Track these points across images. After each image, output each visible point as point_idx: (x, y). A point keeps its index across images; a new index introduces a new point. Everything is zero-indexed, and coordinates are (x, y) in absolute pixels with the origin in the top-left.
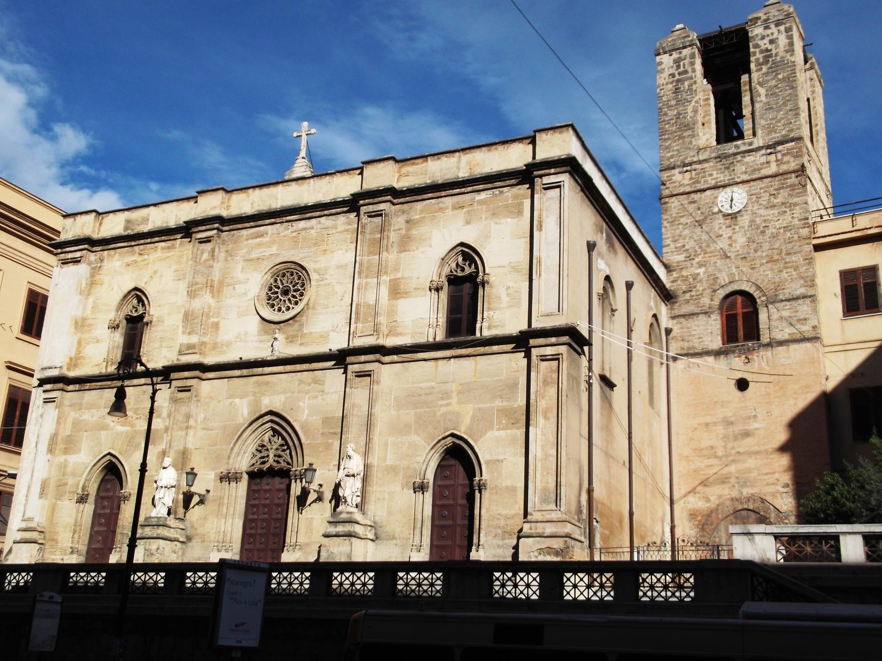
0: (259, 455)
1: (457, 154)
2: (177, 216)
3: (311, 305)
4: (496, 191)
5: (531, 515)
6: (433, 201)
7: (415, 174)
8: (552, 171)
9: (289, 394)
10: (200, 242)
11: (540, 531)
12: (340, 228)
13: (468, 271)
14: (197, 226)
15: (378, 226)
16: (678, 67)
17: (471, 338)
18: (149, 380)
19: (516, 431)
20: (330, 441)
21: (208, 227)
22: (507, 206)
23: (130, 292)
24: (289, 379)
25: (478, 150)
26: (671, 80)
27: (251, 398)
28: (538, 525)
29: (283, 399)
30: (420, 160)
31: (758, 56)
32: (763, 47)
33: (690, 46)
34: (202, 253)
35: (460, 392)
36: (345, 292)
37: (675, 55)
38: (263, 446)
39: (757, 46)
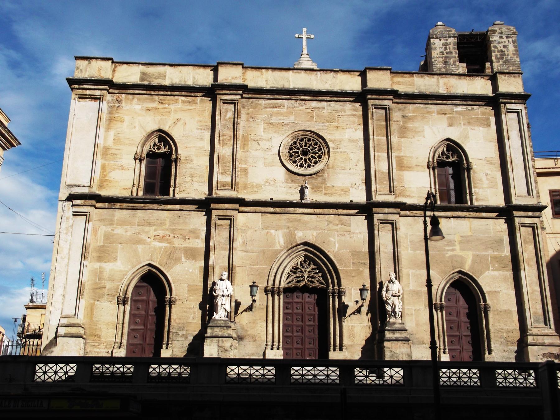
0: (294, 275)
1: (436, 76)
2: (194, 78)
3: (330, 166)
4: (469, 107)
5: (531, 330)
6: (422, 105)
7: (405, 84)
8: (513, 101)
9: (320, 231)
10: (224, 103)
11: (540, 341)
12: (348, 113)
13: (163, 150)
14: (223, 89)
15: (382, 116)
16: (446, 49)
17: (166, 197)
18: (422, 213)
19: (505, 272)
20: (361, 269)
21: (232, 92)
22: (478, 119)
23: (153, 132)
24: (318, 219)
25: (451, 77)
26: (442, 56)
27: (286, 231)
28: (538, 337)
29: (315, 234)
30: (408, 75)
31: (496, 53)
32: (499, 49)
33: (453, 37)
34: (227, 112)
35: (460, 242)
36: (358, 160)
37: (443, 41)
38: (297, 268)
39: (495, 47)
